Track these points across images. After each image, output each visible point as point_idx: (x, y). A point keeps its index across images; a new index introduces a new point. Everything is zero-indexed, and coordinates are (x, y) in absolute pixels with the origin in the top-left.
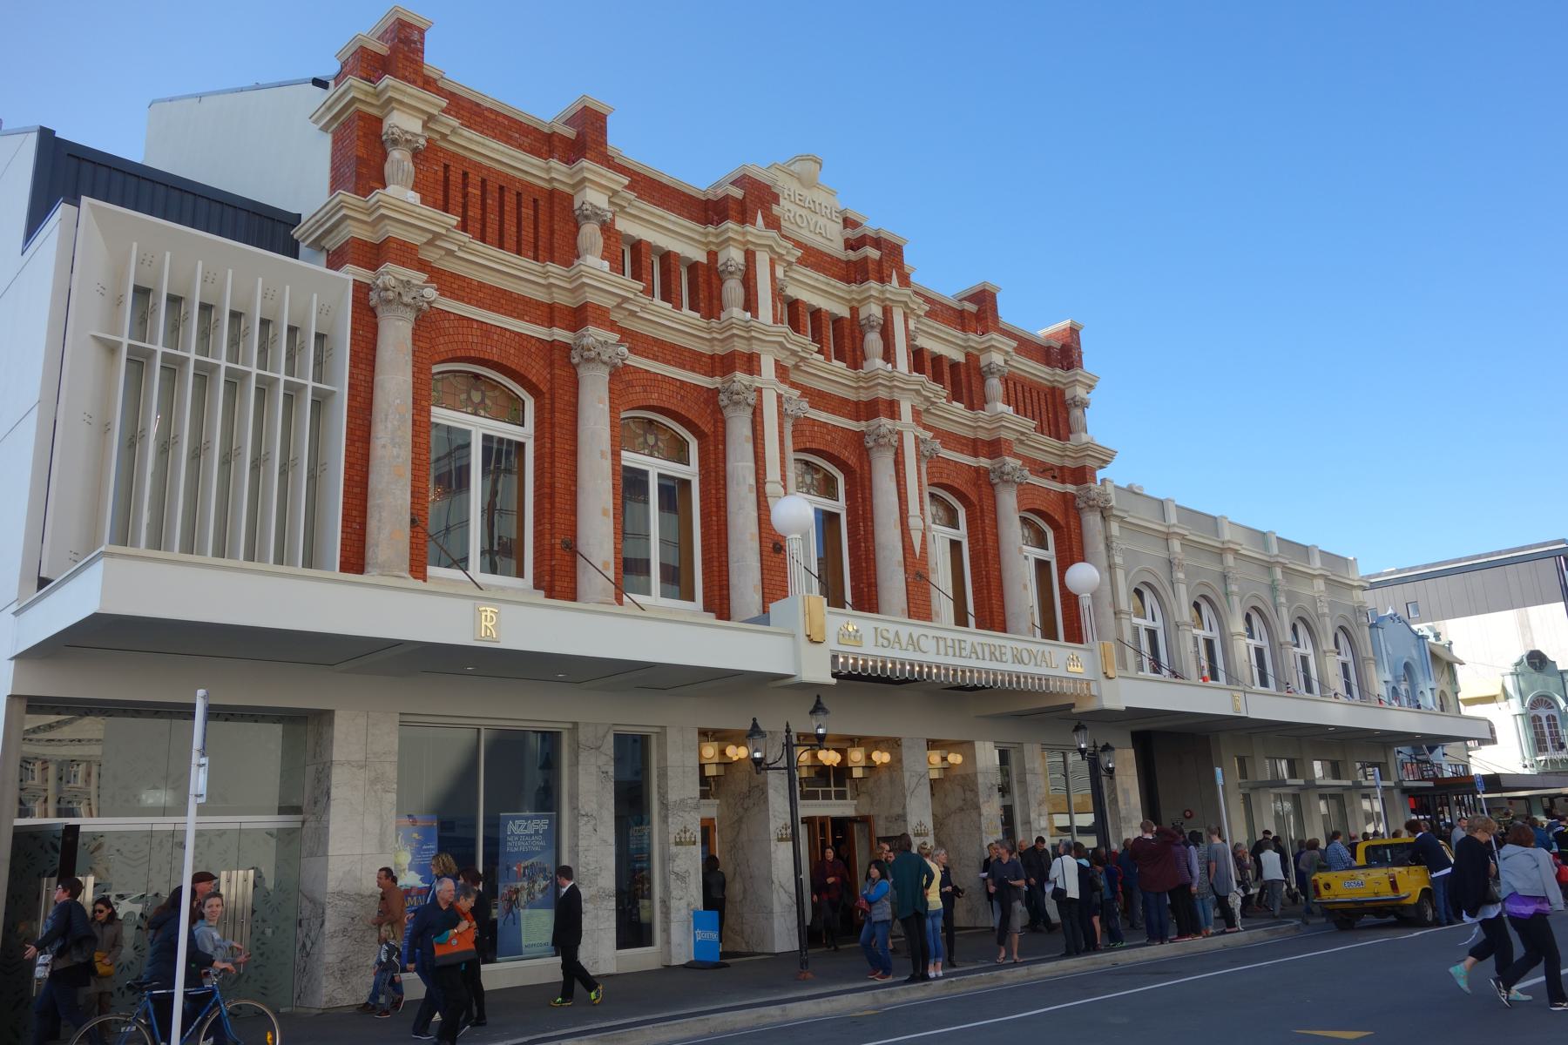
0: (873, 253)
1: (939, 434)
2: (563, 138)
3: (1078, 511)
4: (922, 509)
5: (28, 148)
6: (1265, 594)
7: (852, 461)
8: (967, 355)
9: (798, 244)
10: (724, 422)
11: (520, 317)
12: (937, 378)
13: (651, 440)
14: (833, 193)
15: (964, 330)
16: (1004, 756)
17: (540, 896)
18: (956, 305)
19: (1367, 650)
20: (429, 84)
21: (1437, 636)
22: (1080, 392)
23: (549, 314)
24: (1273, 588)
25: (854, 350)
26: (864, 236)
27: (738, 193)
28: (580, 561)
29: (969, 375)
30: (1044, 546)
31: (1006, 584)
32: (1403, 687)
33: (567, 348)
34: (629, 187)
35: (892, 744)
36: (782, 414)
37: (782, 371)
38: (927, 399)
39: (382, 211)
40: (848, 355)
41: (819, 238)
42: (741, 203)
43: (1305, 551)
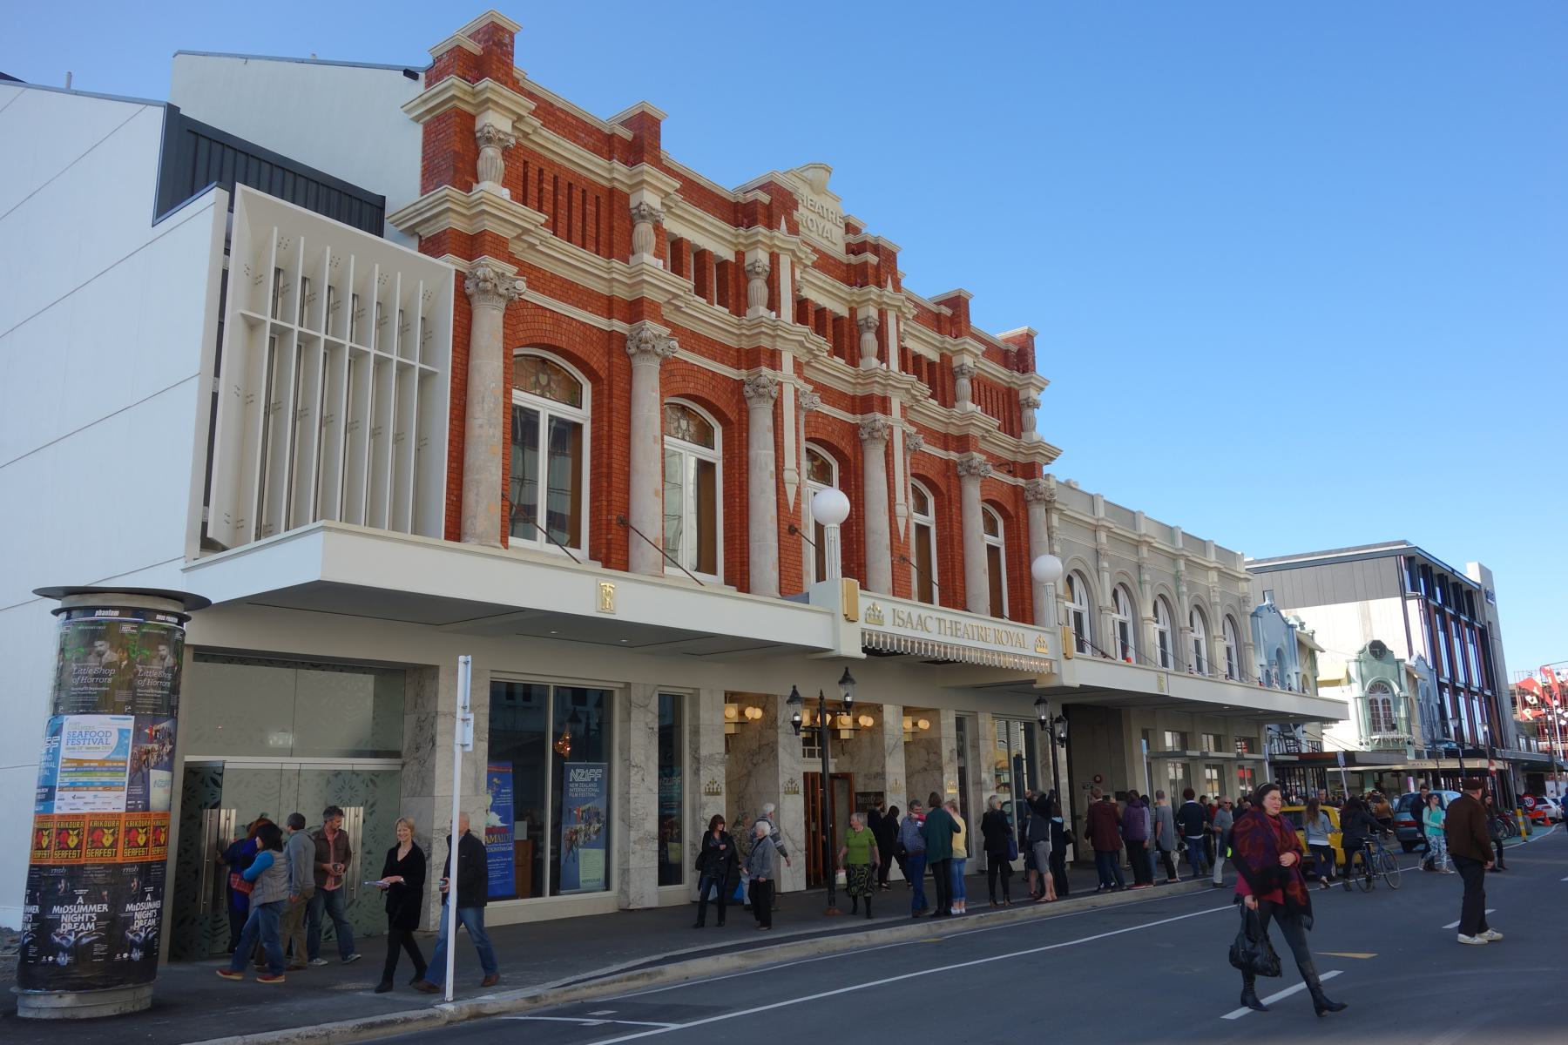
0: (872, 259)
1: (922, 429)
2: (622, 140)
3: (1027, 502)
4: (798, 465)
5: (153, 125)
6: (1169, 583)
7: (848, 451)
8: (942, 356)
9: (815, 250)
10: (748, 412)
11: (584, 308)
12: (819, 329)
13: (543, 379)
14: (837, 199)
15: (940, 332)
16: (960, 724)
17: (594, 837)
18: (934, 308)
19: (1248, 637)
20: (515, 85)
21: (1302, 625)
22: (1033, 393)
23: (609, 306)
24: (1177, 578)
25: (852, 348)
26: (865, 243)
27: (765, 198)
28: (634, 536)
29: (943, 375)
30: (925, 513)
31: (967, 572)
32: (1274, 671)
33: (623, 339)
34: (534, 113)
35: (764, 701)
36: (798, 407)
37: (798, 366)
38: (810, 351)
39: (484, 207)
40: (847, 351)
41: (825, 242)
42: (769, 207)
43: (1202, 545)
